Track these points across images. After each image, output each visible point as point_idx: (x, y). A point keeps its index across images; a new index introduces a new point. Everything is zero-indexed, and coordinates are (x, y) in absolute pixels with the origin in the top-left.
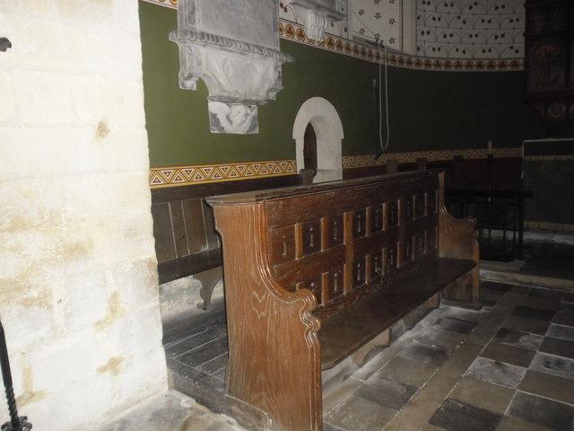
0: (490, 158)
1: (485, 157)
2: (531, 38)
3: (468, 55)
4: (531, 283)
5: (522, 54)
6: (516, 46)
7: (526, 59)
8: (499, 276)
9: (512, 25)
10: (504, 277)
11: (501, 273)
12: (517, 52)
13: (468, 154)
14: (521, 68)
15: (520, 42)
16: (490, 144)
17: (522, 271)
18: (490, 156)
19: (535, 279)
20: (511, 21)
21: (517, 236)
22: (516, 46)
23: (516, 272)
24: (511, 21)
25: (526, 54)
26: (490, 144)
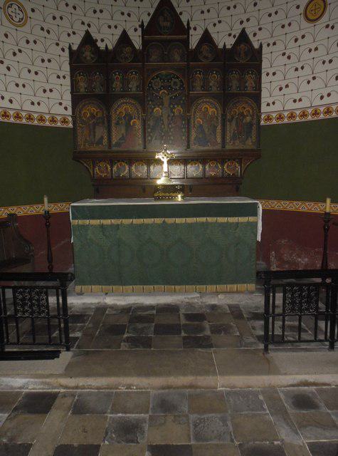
0: (47, 215)
1: (42, 212)
2: (77, 99)
3: (15, 106)
4: (77, 387)
5: (70, 112)
6: (64, 104)
7: (74, 116)
8: (42, 383)
9: (203, 16)
10: (48, 384)
11: (44, 380)
12: (66, 108)
13: (22, 211)
14: (71, 125)
15: (67, 100)
16: (46, 200)
17: (69, 371)
18: (47, 212)
19: (81, 381)
20: (202, 12)
21: (235, 84)
22: (64, 104)
23: (60, 376)
24: (202, 12)
25: (73, 112)
26: (46, 200)
